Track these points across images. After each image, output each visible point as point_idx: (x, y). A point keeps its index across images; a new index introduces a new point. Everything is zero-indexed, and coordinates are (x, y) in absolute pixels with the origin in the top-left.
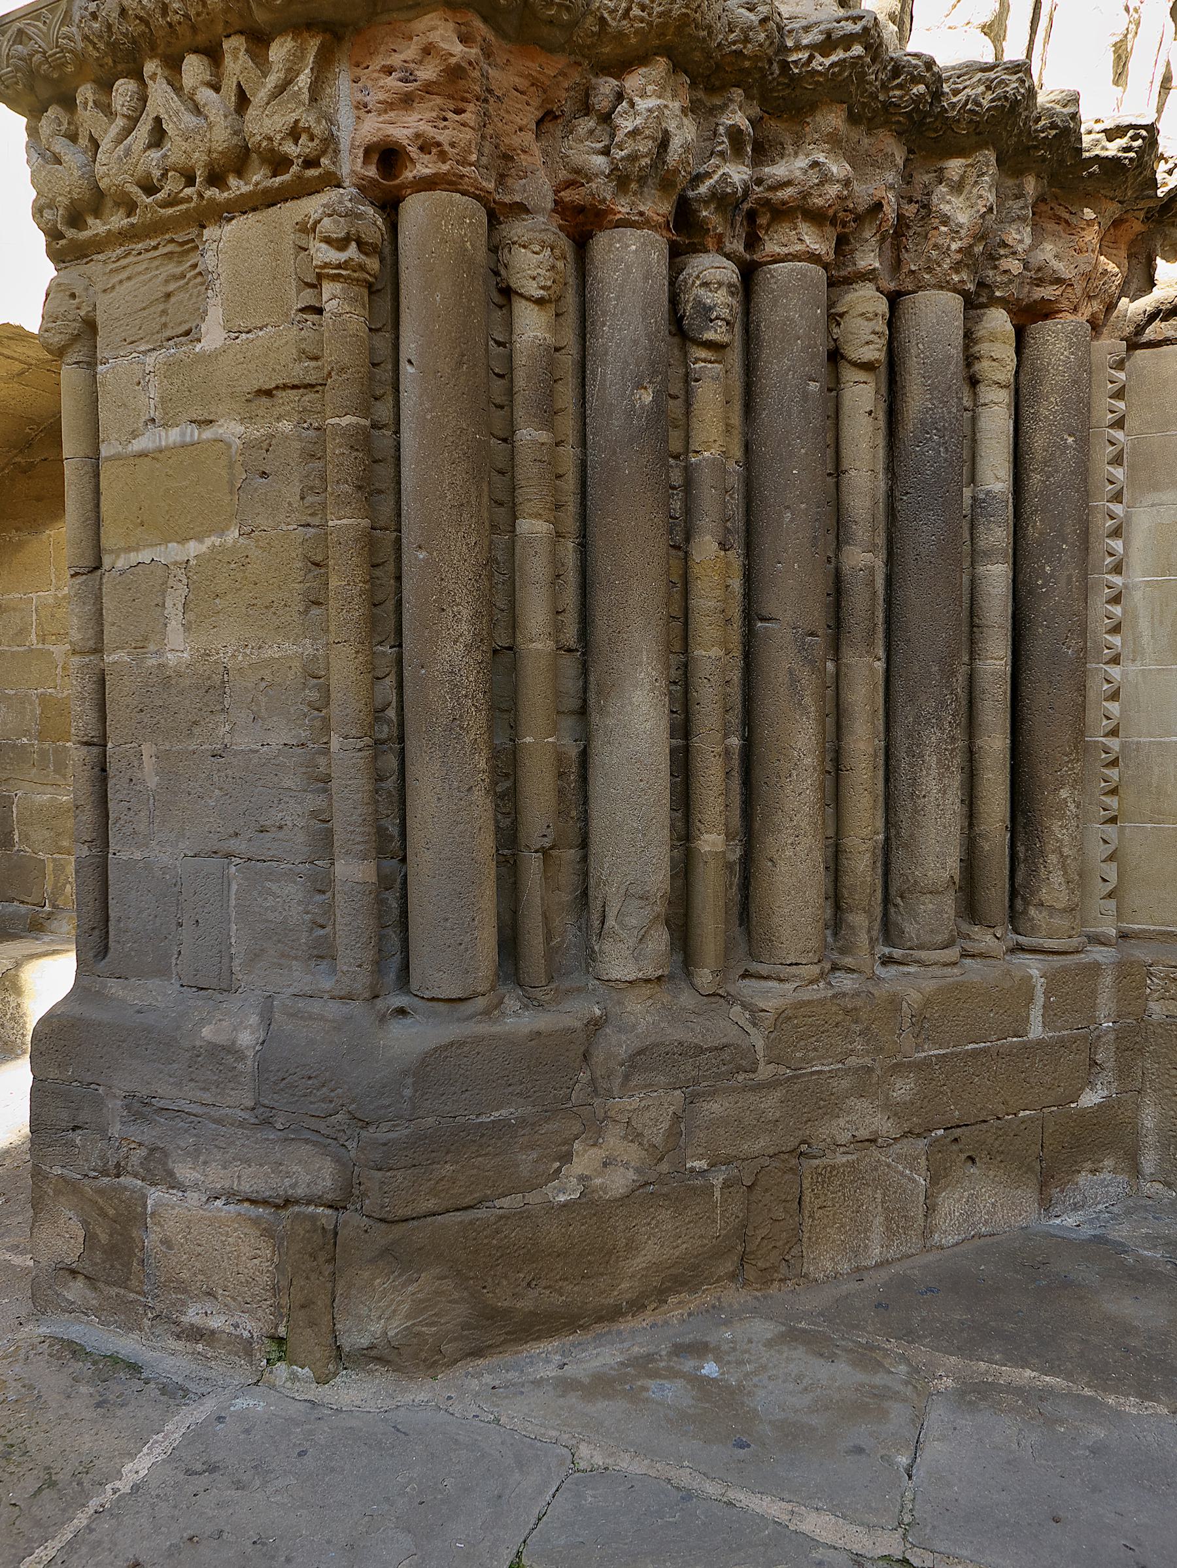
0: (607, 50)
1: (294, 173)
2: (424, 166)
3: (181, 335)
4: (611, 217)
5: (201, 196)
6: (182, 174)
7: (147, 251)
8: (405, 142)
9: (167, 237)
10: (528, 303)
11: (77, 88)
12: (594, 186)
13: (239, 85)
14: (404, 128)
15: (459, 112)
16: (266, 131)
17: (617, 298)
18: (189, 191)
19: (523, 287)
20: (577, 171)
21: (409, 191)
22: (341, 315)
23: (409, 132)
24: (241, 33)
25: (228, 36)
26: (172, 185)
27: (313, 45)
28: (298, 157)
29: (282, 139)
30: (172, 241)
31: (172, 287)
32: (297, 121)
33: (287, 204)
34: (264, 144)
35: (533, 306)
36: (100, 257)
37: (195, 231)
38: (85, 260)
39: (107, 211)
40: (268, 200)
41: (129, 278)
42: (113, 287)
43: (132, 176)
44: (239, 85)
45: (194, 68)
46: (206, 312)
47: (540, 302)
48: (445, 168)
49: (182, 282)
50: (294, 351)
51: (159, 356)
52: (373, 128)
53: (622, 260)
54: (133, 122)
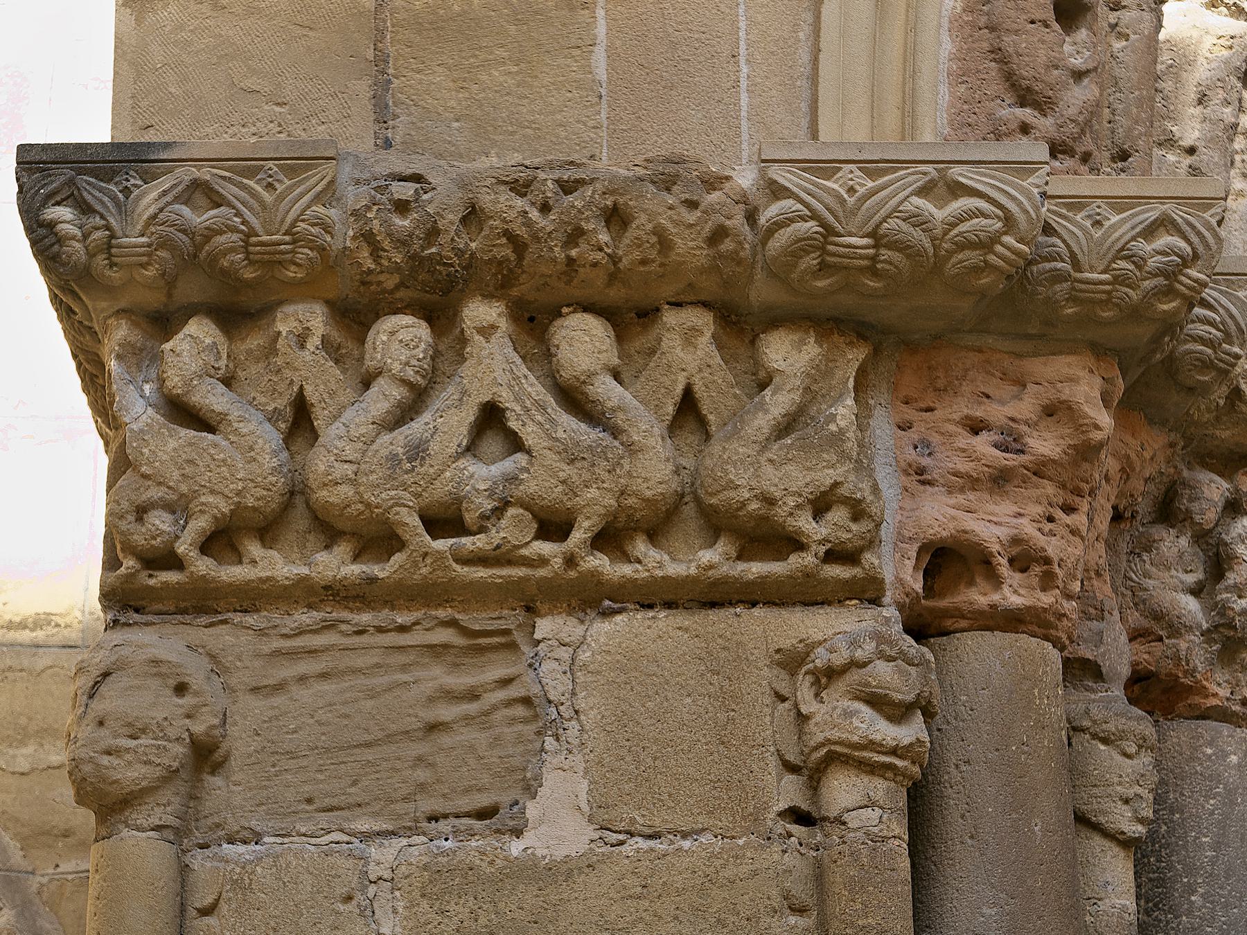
0: (1225, 434)
1: (767, 556)
2: (1015, 593)
3: (468, 815)
4: (1197, 700)
5: (570, 561)
6: (535, 516)
7: (380, 630)
8: (995, 548)
9: (442, 613)
10: (1107, 844)
11: (280, 303)
12: (1183, 645)
13: (688, 392)
14: (992, 523)
15: (1069, 509)
16: (766, 485)
17: (1216, 846)
18: (545, 548)
19: (1104, 813)
20: (1158, 616)
21: (964, 624)
22: (884, 839)
23: (1003, 533)
24: (705, 305)
25: (678, 305)
26: (512, 530)
27: (856, 356)
28: (821, 542)
29: (798, 506)
30: (452, 623)
31: (446, 712)
32: (836, 485)
33: (756, 611)
34: (754, 506)
35: (1116, 849)
36: (250, 619)
37: (521, 615)
38: (204, 620)
39: (291, 536)
40: (712, 596)
41: (324, 676)
42: (280, 687)
43: (418, 496)
44: (688, 392)
45: (583, 342)
46: (538, 778)
47: (1126, 843)
48: (1047, 599)
49: (472, 708)
50: (774, 892)
51: (417, 849)
52: (940, 514)
53: (1218, 778)
54: (416, 400)
